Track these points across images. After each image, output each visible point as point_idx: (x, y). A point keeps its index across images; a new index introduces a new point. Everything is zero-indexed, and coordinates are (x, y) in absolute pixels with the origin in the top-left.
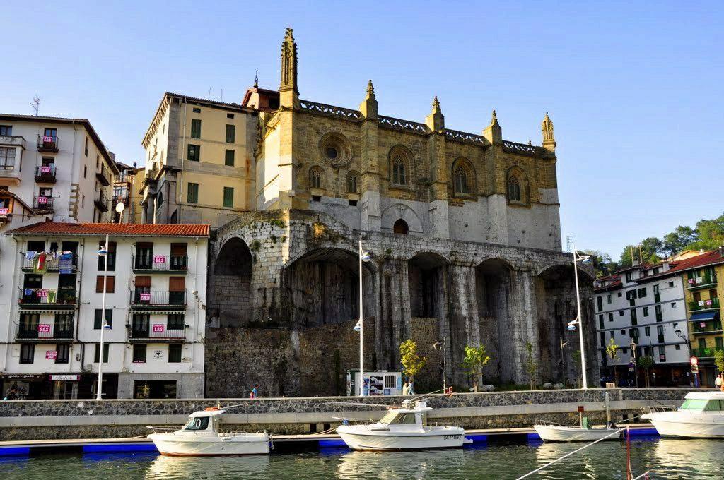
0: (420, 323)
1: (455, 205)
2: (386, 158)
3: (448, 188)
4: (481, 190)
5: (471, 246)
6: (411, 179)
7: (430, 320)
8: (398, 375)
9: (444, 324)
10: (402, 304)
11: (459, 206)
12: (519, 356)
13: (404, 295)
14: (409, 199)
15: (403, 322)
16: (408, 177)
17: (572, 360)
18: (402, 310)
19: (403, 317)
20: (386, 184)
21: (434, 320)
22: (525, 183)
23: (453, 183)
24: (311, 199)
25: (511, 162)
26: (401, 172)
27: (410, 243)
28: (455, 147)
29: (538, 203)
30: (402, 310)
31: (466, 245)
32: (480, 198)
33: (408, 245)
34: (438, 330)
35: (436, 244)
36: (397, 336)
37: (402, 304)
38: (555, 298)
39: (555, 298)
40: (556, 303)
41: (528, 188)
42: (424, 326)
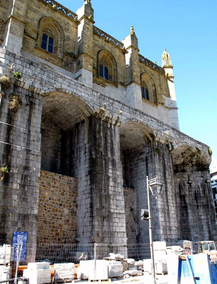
0: (54, 179)
1: (99, 84)
2: (36, 22)
3: (94, 68)
4: (120, 80)
5: (117, 103)
6: (59, 49)
7: (66, 178)
8: (60, 242)
9: (84, 182)
10: (28, 144)
11: (102, 86)
12: (162, 227)
13: (32, 133)
14: (55, 64)
15: (26, 168)
16: (56, 48)
17: (196, 235)
18: (28, 151)
19: (27, 160)
20: (32, 43)
21: (72, 179)
22: (153, 88)
23: (98, 66)
25: (143, 69)
26: (49, 43)
27: (48, 76)
28: (101, 42)
29: (163, 104)
30: (28, 151)
31: (111, 101)
32: (119, 86)
33: (45, 77)
34: (75, 191)
35: (79, 88)
36: (15, 186)
37: (28, 144)
38: (179, 180)
39: (179, 180)
40: (180, 184)
41: (155, 92)
42: (57, 184)
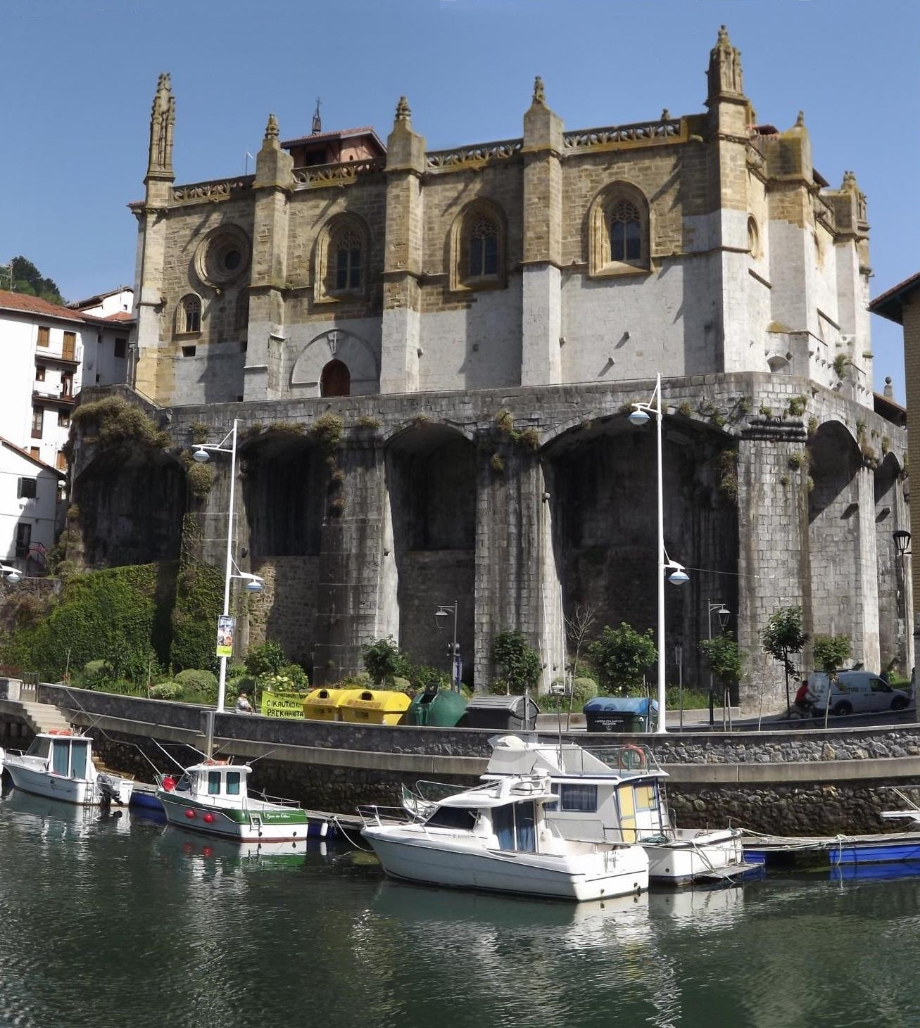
24: (181, 354)
